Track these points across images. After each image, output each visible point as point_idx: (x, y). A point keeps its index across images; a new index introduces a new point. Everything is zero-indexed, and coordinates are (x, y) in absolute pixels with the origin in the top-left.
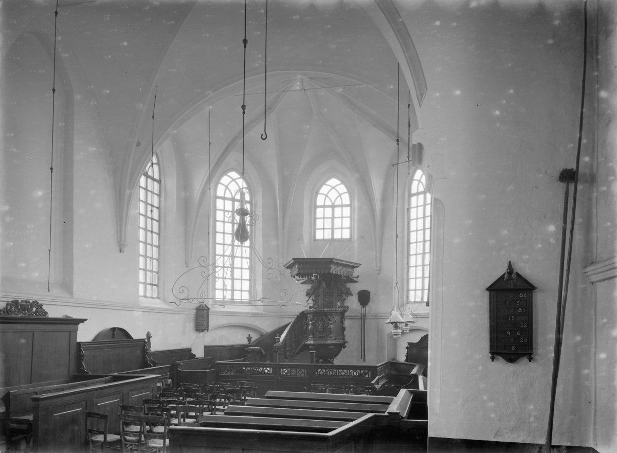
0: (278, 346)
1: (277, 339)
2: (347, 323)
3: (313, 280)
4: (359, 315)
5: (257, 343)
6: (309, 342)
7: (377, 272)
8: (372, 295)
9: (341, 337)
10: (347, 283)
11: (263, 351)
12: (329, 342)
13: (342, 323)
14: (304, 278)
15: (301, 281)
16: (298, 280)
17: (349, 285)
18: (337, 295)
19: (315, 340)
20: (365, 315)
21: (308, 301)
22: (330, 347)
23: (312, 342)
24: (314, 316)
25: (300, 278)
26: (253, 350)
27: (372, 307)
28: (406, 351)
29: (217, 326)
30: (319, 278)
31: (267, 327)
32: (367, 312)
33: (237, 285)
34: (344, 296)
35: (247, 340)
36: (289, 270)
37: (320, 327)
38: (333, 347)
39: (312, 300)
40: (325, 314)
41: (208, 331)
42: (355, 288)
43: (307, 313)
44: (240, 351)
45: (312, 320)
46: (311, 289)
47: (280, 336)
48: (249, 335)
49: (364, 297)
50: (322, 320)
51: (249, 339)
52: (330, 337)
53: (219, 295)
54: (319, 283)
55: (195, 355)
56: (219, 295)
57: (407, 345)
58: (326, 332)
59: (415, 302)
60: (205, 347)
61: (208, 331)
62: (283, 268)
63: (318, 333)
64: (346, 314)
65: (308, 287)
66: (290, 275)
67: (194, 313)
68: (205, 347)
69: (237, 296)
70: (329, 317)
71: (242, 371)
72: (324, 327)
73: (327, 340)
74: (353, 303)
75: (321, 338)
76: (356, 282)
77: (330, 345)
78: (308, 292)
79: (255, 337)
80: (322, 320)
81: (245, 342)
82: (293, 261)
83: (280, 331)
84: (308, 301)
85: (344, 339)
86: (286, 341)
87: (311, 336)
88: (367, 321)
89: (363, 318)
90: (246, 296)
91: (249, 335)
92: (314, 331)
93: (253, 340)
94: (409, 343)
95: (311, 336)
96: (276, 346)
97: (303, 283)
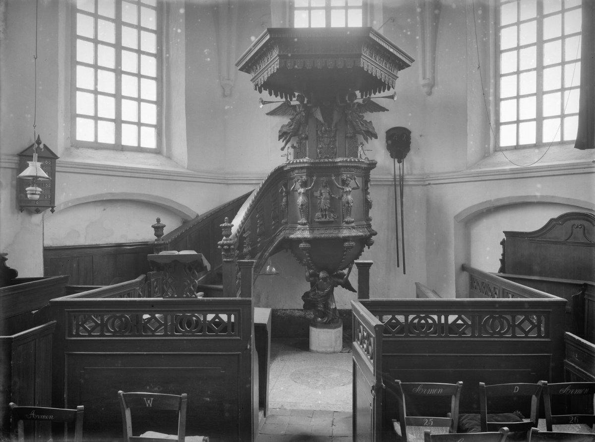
0: (229, 245)
1: (225, 227)
2: (374, 195)
3: (294, 106)
4: (391, 177)
5: (177, 242)
6: (298, 235)
7: (426, 89)
8: (414, 136)
9: (364, 223)
10: (366, 111)
11: (206, 263)
12: (345, 233)
13: (365, 191)
14: (279, 97)
15: (274, 106)
16: (264, 103)
17: (369, 116)
18: (346, 137)
19: (312, 229)
20: (402, 178)
21: (283, 149)
22: (346, 244)
23: (307, 234)
24: (310, 175)
25: (271, 94)
26: (176, 261)
27: (417, 162)
28: (500, 250)
29: (78, 199)
30: (305, 102)
31: (198, 202)
32: (405, 172)
33: (129, 110)
34: (361, 138)
35: (153, 231)
36: (249, 77)
37: (323, 201)
38: (353, 243)
39: (293, 147)
40: (336, 169)
41: (53, 211)
42: (383, 122)
43: (289, 171)
44: (133, 260)
45: (304, 184)
46: (290, 125)
47: (230, 221)
48: (158, 220)
49: (399, 143)
50: (330, 184)
51: (158, 229)
52: (347, 223)
53: (84, 131)
54: (309, 114)
55: (14, 273)
56: (84, 131)
57: (503, 237)
58: (337, 211)
59: (518, 147)
60: (47, 250)
61: (53, 211)
62: (234, 70)
63: (318, 214)
64: (373, 174)
65: (284, 121)
66: (252, 85)
67: (14, 166)
68: (47, 250)
69: (129, 137)
70: (344, 177)
71: (138, 326)
72: (332, 199)
73: (339, 228)
74: (376, 151)
75: (325, 224)
76: (383, 109)
77: (346, 239)
78: (285, 130)
79: (170, 225)
80: (330, 184)
81: (149, 236)
82: (268, 37)
83: (232, 208)
84: (283, 149)
85: (369, 226)
86: (244, 232)
87: (304, 221)
88: (406, 190)
89: (399, 183)
90: (149, 140)
91: (158, 220)
92: (310, 208)
93: (166, 231)
94: (507, 233)
95: (304, 221)
96: (223, 245)
97: (272, 113)
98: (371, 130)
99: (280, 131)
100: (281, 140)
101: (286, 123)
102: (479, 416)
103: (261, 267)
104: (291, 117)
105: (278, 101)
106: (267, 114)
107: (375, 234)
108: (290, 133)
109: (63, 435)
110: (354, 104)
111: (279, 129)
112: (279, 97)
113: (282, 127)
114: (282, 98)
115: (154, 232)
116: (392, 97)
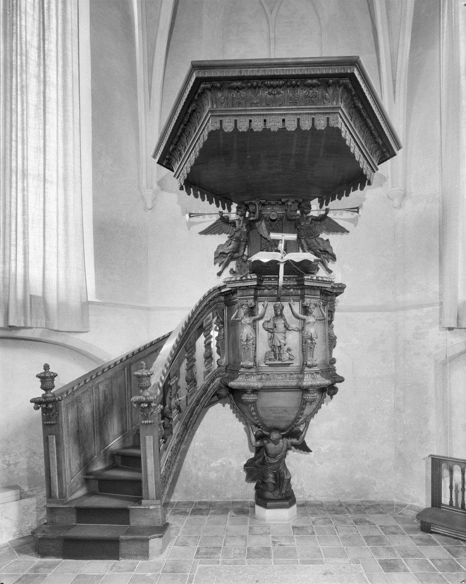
21: (219, 274)
35: (38, 383)
46: (228, 243)
48: (46, 367)
84: (219, 274)
91: (46, 367)
93: (59, 383)
98: (328, 250)
99: (215, 253)
100: (218, 265)
101: (224, 243)
102: (304, 397)
103: (226, 293)
104: (229, 235)
105: (210, 212)
106: (201, 233)
107: (341, 380)
108: (228, 254)
109: (83, 475)
110: (308, 217)
111: (215, 249)
112: (214, 205)
113: (218, 247)
114: (218, 206)
115: (40, 384)
116: (356, 210)
